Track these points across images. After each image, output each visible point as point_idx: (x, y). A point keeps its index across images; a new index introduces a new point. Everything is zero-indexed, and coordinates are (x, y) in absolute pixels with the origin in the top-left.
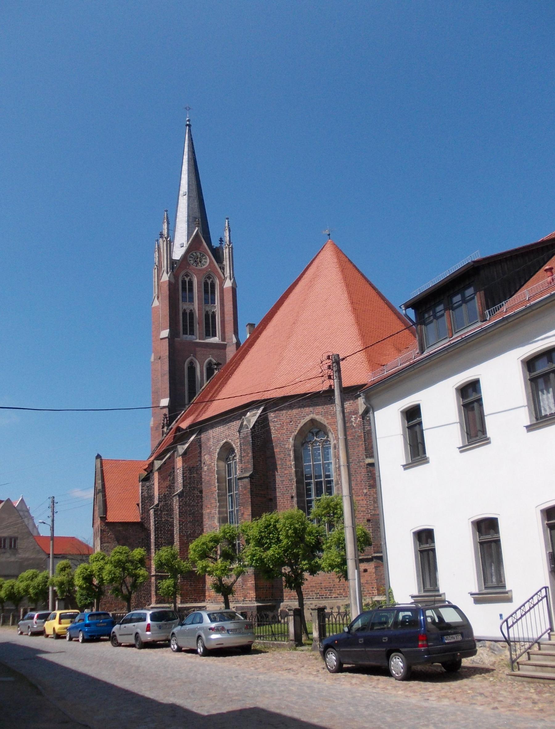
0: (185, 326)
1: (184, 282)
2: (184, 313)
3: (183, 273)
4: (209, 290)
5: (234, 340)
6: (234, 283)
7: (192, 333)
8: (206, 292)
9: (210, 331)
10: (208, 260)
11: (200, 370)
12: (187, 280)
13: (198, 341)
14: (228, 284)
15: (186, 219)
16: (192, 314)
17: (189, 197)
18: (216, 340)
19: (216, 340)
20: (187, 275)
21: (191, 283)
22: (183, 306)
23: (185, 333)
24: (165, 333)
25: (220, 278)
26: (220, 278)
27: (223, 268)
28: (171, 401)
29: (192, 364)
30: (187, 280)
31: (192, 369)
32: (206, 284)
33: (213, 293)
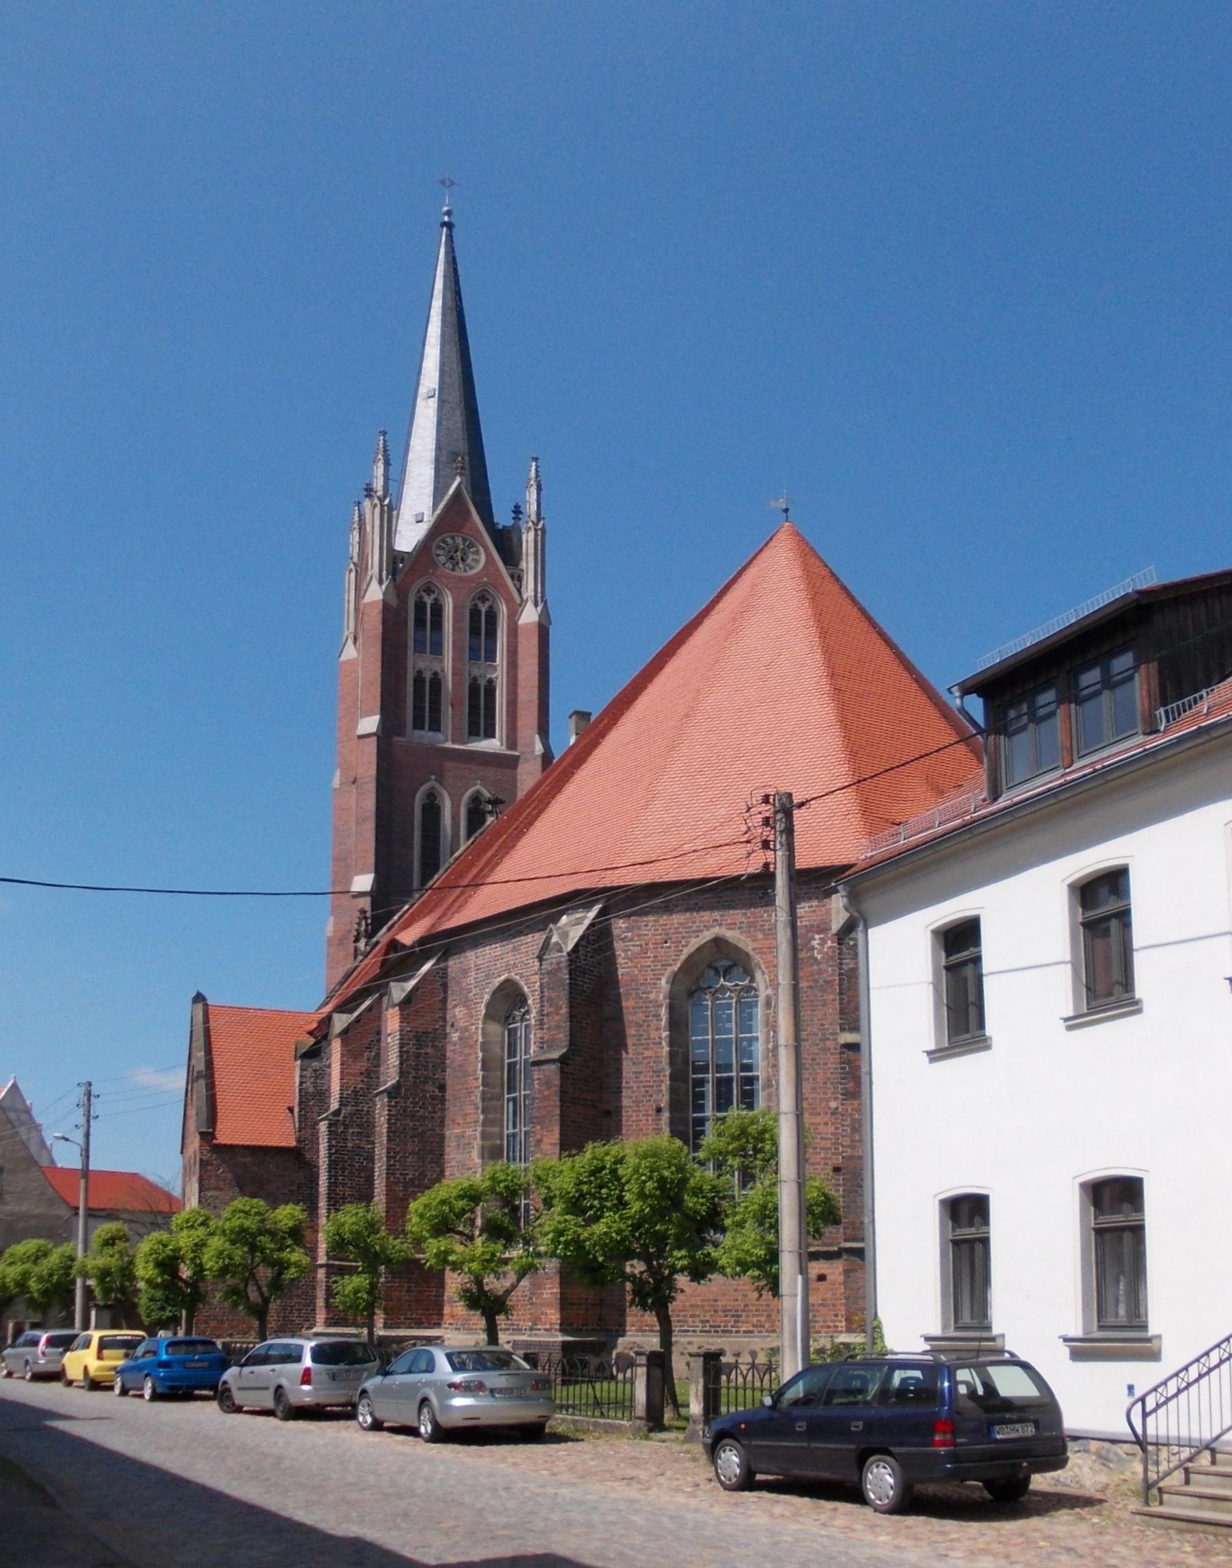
0: (418, 709)
1: (420, 606)
2: (419, 680)
3: (419, 583)
4: (481, 628)
5: (539, 748)
6: (545, 616)
7: (436, 726)
8: (474, 631)
9: (480, 724)
10: (483, 556)
11: (450, 814)
12: (429, 600)
13: (449, 745)
14: (529, 615)
15: (431, 455)
16: (436, 682)
17: (442, 403)
18: (493, 745)
19: (493, 745)
20: (429, 591)
21: (438, 610)
22: (416, 663)
23: (419, 724)
24: (370, 724)
25: (510, 601)
26: (510, 601)
27: (518, 578)
28: (377, 882)
29: (432, 796)
30: (429, 600)
31: (432, 811)
32: (475, 613)
33: (492, 634)
